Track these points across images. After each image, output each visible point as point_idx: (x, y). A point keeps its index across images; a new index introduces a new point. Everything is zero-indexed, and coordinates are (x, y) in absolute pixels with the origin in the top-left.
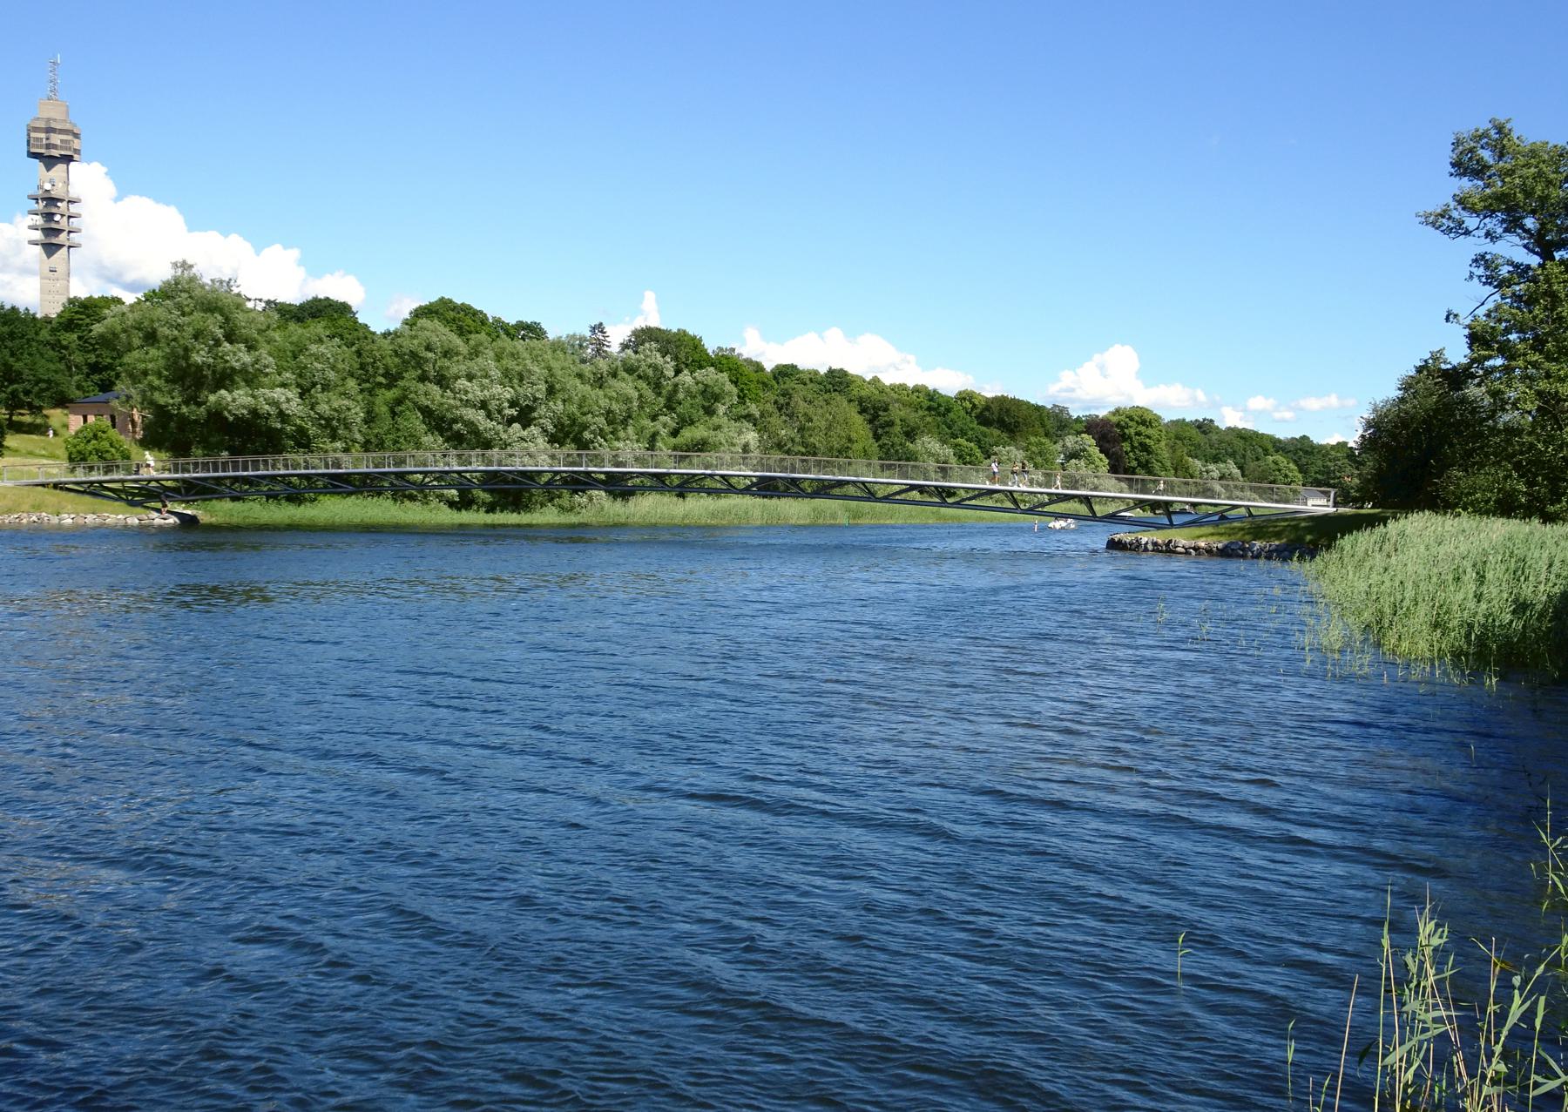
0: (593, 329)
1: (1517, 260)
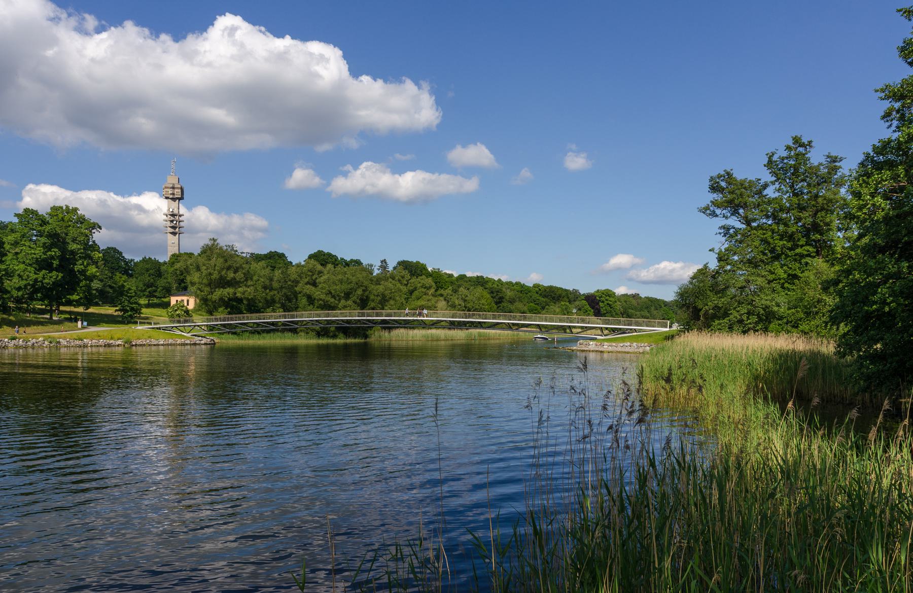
1: (736, 226)
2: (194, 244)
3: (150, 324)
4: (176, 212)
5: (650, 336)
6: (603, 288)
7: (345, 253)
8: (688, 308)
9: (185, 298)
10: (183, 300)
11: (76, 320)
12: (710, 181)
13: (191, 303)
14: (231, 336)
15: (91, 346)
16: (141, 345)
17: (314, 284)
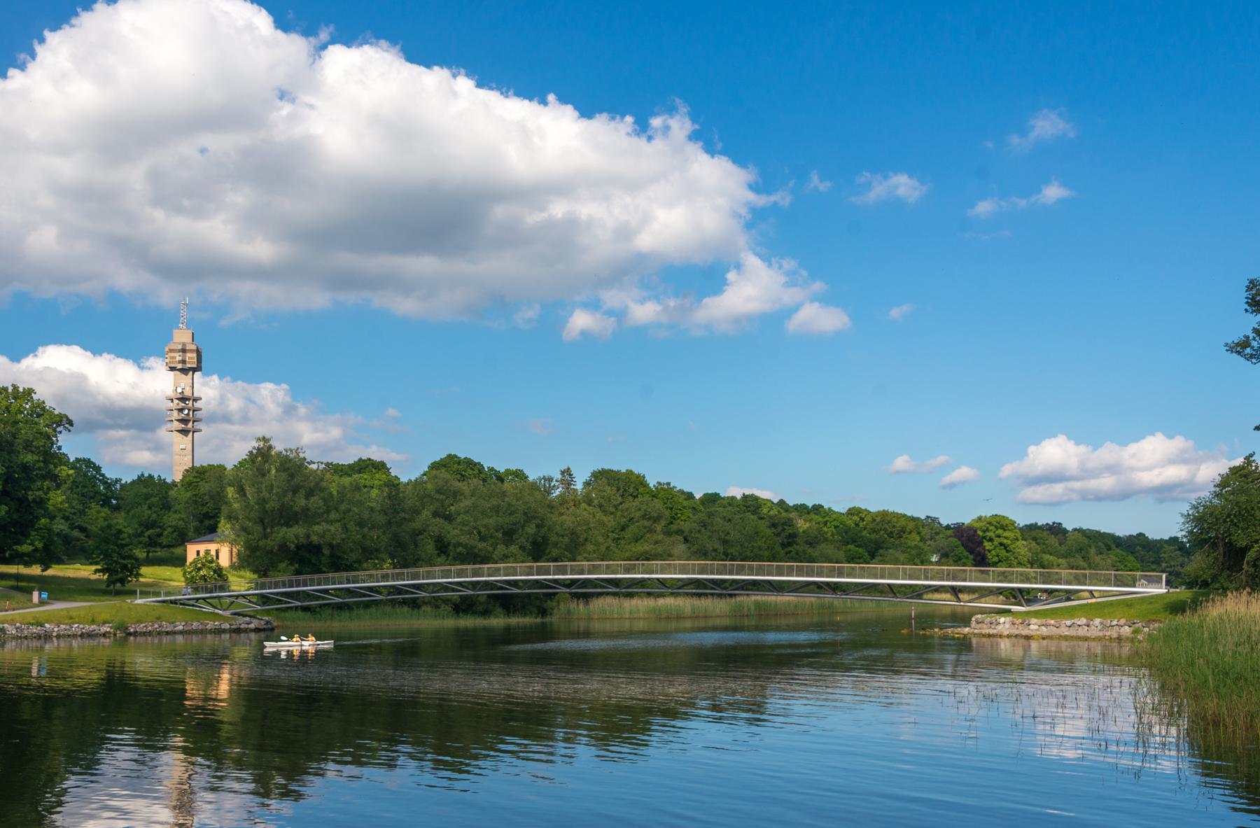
0: (563, 473)
2: (231, 452)
3: (157, 594)
4: (188, 393)
5: (1129, 604)
6: (987, 512)
7: (494, 459)
8: (1214, 545)
9: (213, 547)
10: (208, 552)
11: (29, 591)
12: (1249, 289)
13: (224, 554)
14: (300, 613)
15: (58, 637)
16: (144, 634)
17: (449, 518)
